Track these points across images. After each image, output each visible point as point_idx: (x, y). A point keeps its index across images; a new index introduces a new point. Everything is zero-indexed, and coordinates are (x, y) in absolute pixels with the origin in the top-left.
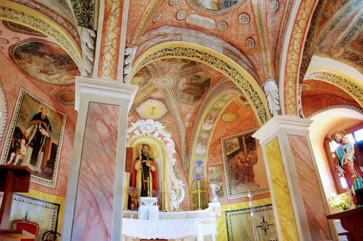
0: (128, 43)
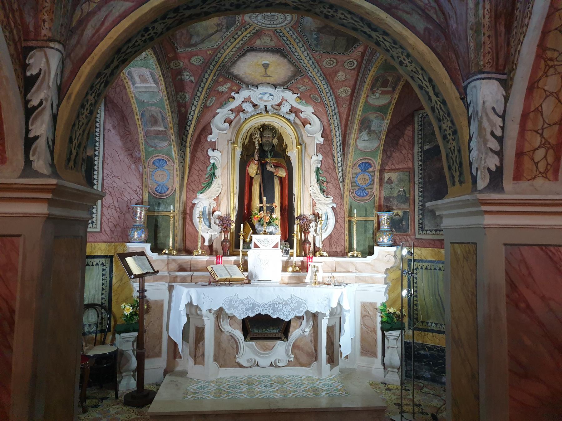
0: (32, 35)
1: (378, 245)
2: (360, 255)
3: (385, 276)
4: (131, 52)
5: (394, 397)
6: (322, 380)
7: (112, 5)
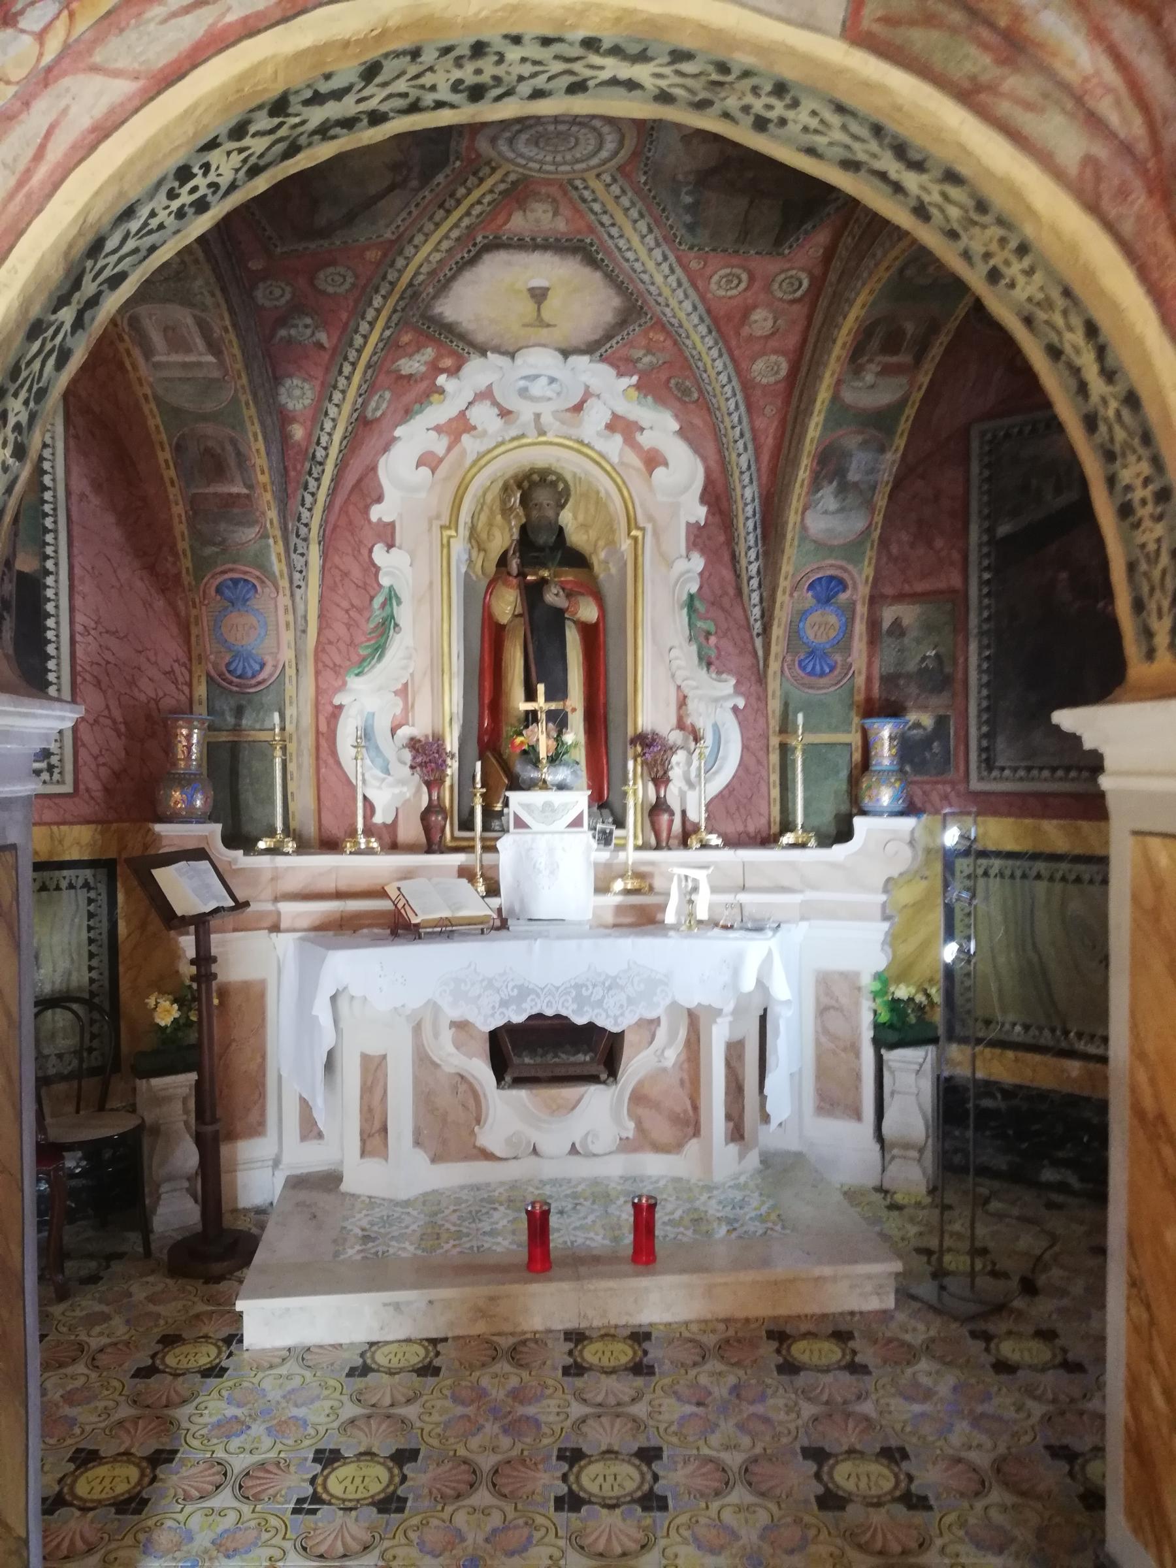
1: (863, 813)
2: (812, 842)
3: (883, 898)
4: (136, 251)
5: (912, 1230)
6: (716, 1188)
7: (68, 90)
